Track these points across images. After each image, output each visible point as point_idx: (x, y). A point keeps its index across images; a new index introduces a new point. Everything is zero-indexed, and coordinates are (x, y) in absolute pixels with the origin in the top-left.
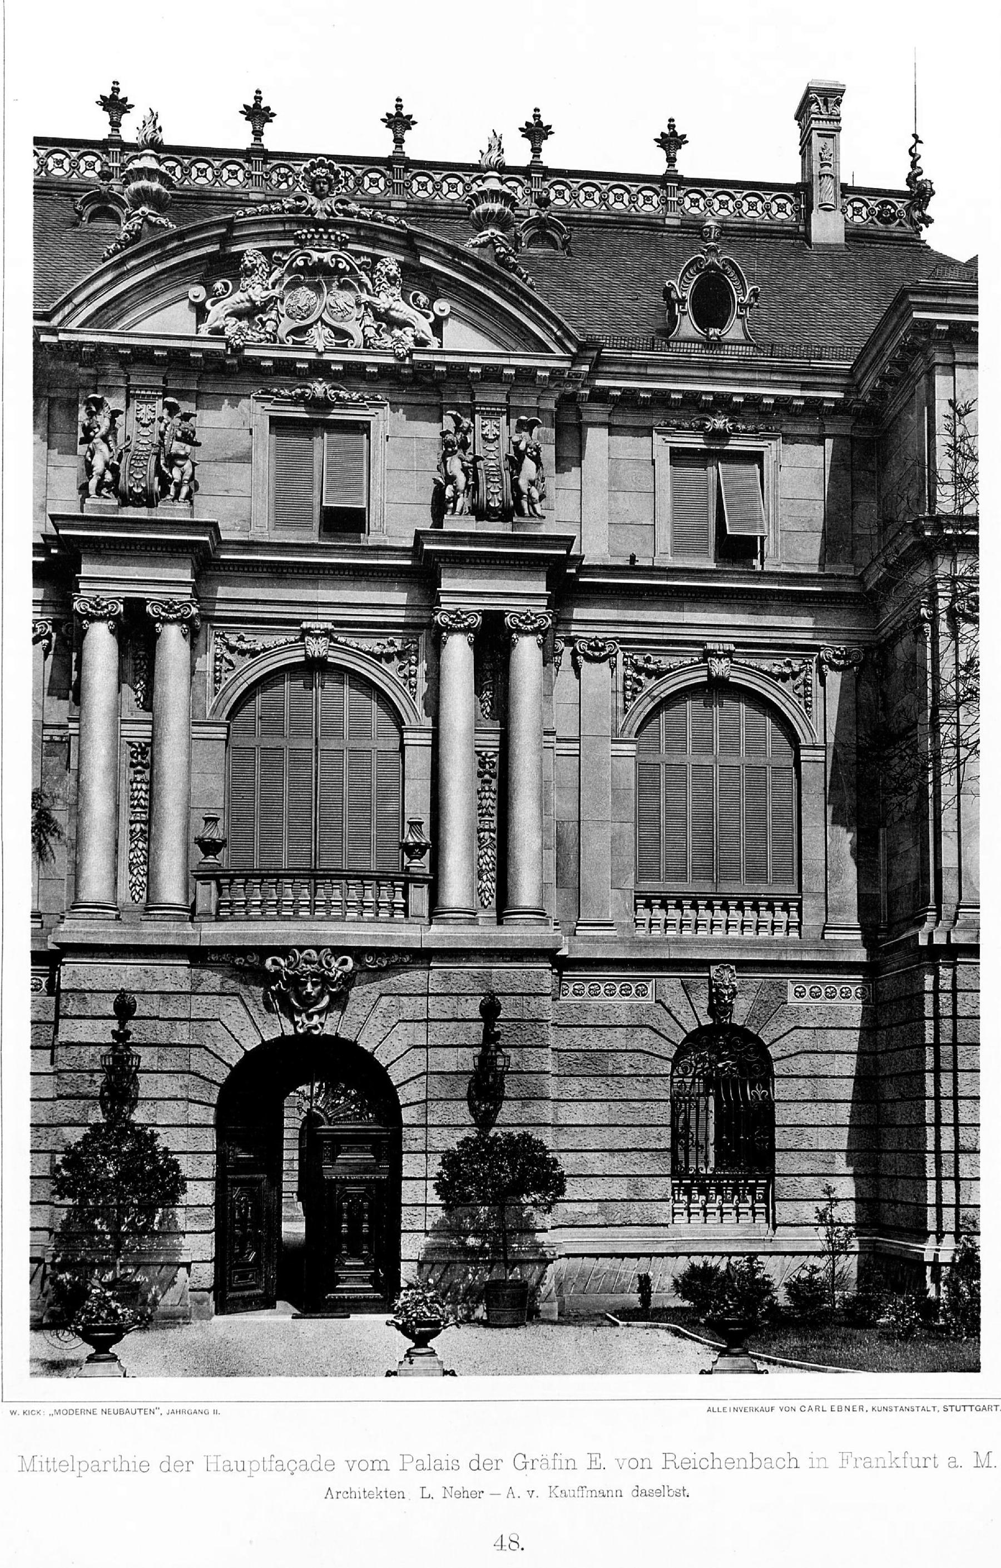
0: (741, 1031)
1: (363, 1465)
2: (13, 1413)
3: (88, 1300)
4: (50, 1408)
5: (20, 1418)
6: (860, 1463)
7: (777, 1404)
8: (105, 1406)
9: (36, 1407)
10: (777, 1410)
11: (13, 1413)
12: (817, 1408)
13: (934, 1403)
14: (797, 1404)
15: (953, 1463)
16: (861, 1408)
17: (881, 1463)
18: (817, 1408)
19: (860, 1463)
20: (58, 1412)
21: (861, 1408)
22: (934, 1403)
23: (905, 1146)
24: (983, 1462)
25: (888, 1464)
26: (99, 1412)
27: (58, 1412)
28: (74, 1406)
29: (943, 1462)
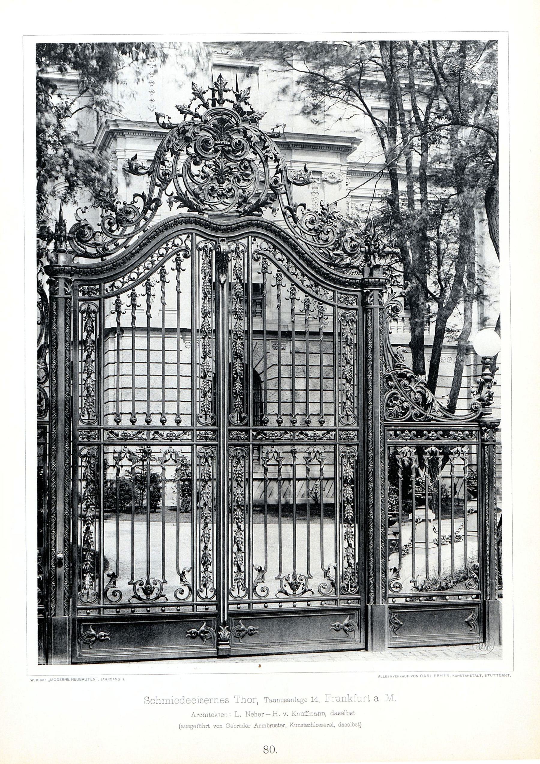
0: (459, 252)
1: (250, 701)
2: (32, 680)
3: (83, 618)
4: (48, 678)
5: (35, 682)
6: (335, 700)
7: (410, 674)
8: (73, 677)
9: (42, 678)
10: (410, 676)
11: (32, 680)
12: (428, 676)
13: (480, 673)
14: (419, 674)
15: (377, 699)
16: (448, 675)
17: (344, 700)
18: (428, 676)
19: (335, 700)
20: (52, 680)
21: (448, 675)
22: (480, 673)
23: (156, 342)
24: (391, 698)
25: (347, 700)
26: (70, 679)
27: (52, 680)
28: (59, 677)
29: (372, 698)
